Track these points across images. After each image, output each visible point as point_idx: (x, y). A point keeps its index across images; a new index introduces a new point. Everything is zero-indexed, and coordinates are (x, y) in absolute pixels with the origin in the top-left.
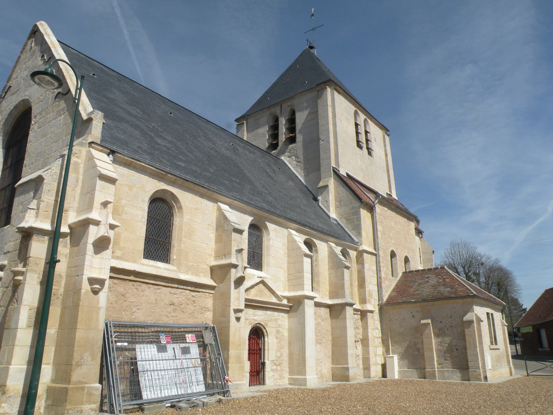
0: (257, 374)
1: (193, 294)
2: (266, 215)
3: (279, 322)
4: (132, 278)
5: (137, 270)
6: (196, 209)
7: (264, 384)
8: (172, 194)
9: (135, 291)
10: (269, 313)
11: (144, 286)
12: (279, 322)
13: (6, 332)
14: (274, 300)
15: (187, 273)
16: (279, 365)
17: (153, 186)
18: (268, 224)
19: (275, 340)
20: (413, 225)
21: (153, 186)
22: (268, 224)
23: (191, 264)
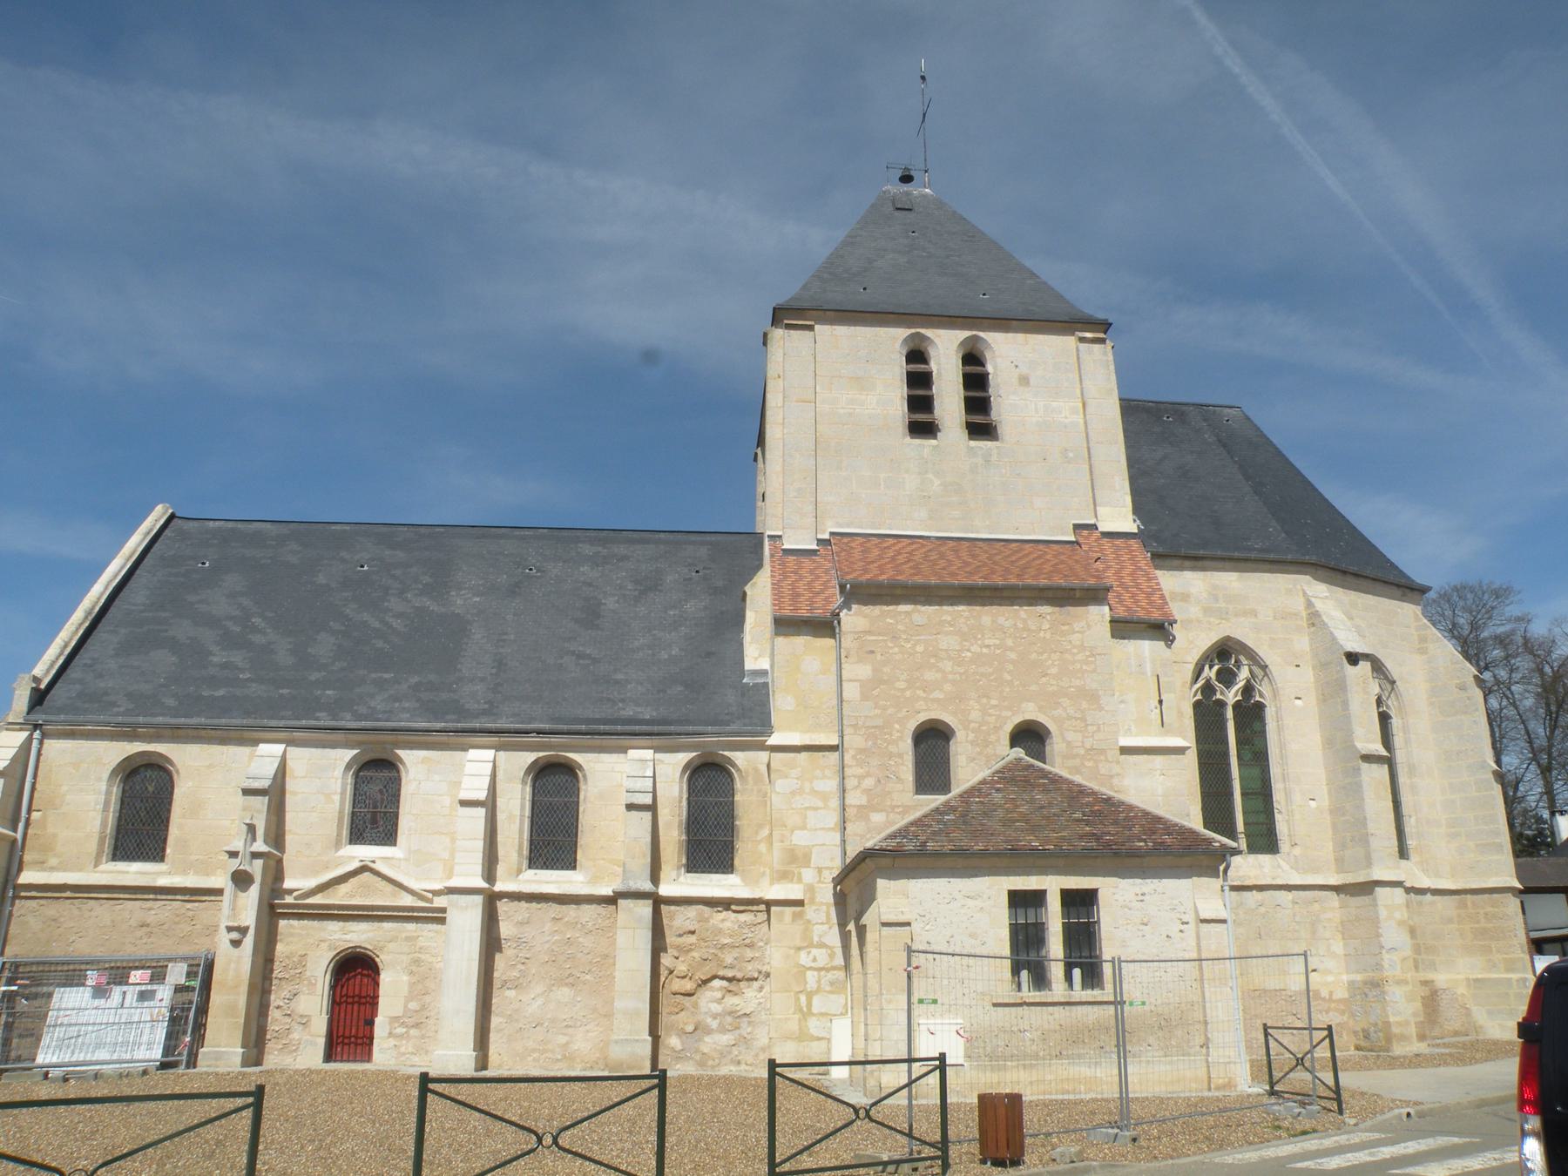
0: (256, 1041)
1: (189, 905)
2: (389, 738)
3: (421, 942)
4: (68, 894)
5: (70, 882)
6: (210, 766)
7: (368, 1057)
8: (161, 755)
9: (76, 912)
10: (387, 925)
11: (92, 902)
12: (421, 942)
13: (684, 861)
14: (408, 900)
15: (184, 872)
16: (417, 1025)
17: (117, 751)
18: (400, 752)
19: (405, 978)
20: (1098, 616)
21: (117, 751)
22: (400, 752)
23: (193, 858)
